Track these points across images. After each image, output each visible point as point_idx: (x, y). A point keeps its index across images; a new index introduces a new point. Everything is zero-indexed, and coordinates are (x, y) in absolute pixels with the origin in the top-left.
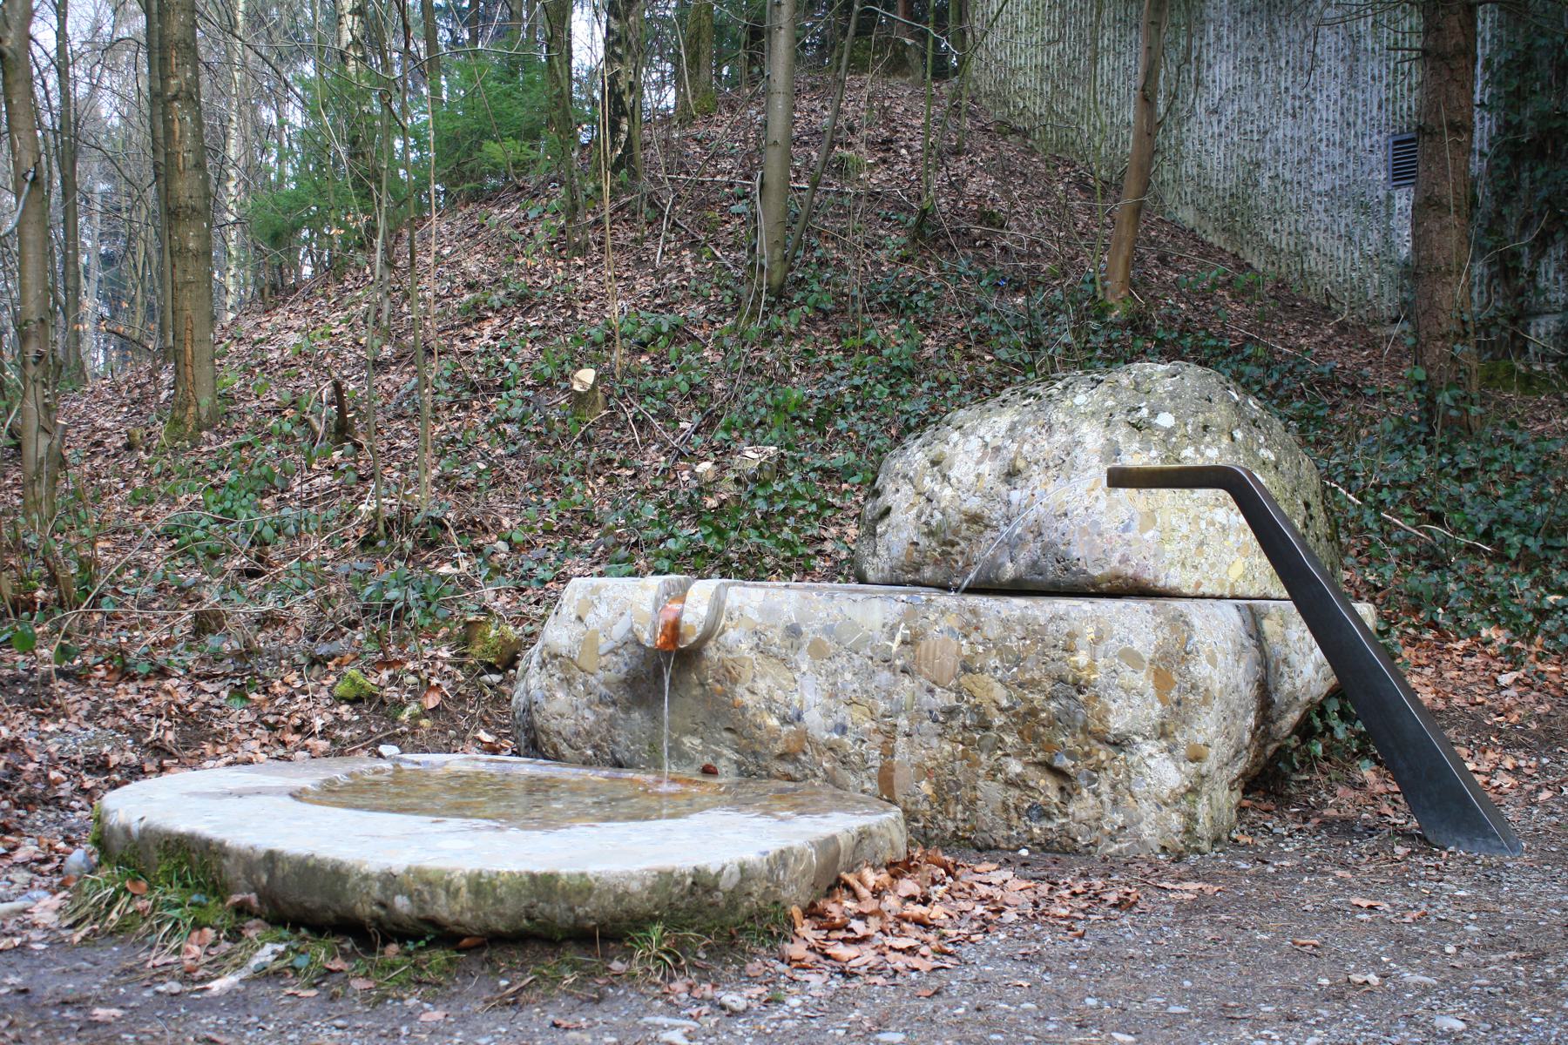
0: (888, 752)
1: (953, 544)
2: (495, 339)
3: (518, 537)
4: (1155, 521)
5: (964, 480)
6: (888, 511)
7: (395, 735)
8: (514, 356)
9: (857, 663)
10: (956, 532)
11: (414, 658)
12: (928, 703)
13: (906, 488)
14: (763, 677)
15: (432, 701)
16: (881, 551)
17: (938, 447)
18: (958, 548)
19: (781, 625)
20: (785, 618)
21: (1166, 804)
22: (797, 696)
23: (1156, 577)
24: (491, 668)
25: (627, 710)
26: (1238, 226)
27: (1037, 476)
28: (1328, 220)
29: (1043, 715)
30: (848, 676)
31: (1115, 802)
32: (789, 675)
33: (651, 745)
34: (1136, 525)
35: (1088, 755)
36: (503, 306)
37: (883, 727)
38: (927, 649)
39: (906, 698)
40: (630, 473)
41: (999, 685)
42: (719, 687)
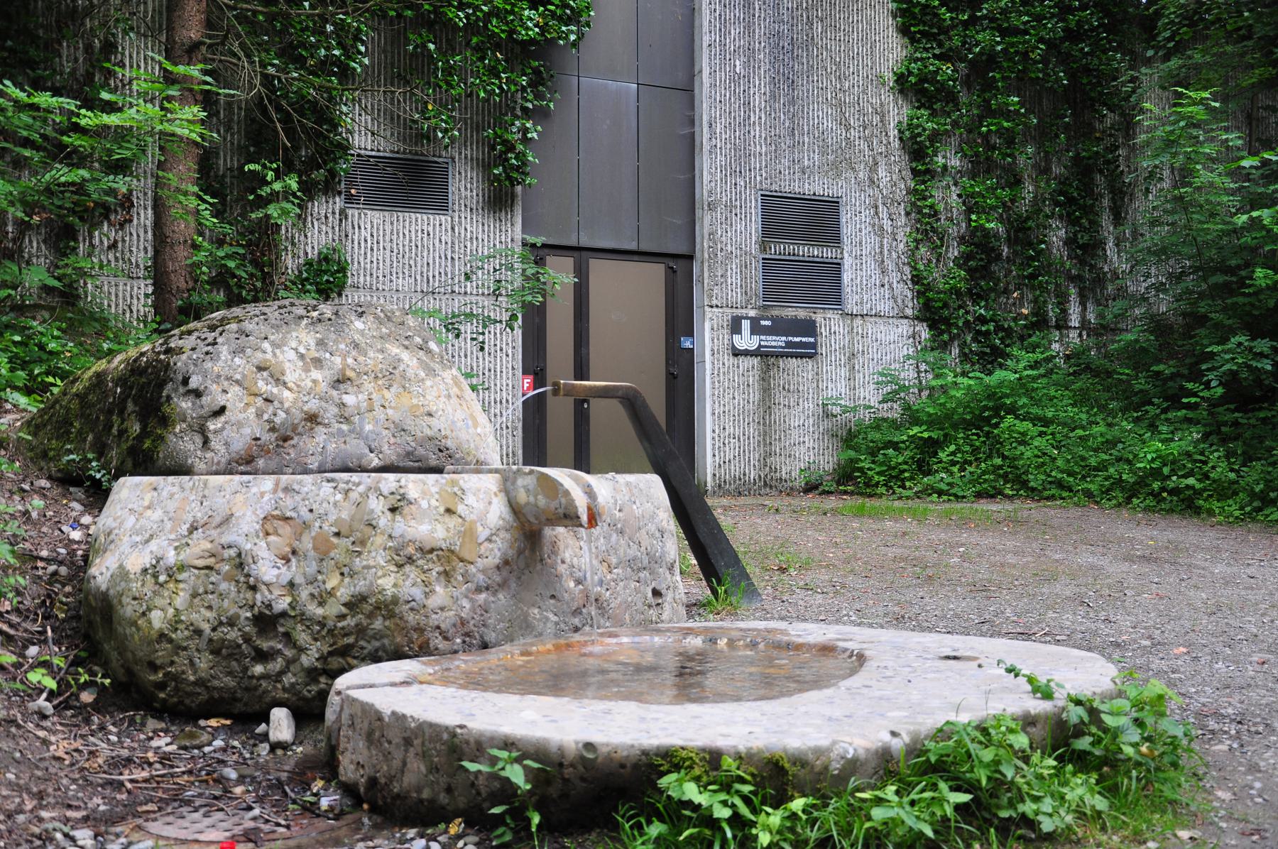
6: (222, 410)
16: (215, 443)
27: (369, 386)
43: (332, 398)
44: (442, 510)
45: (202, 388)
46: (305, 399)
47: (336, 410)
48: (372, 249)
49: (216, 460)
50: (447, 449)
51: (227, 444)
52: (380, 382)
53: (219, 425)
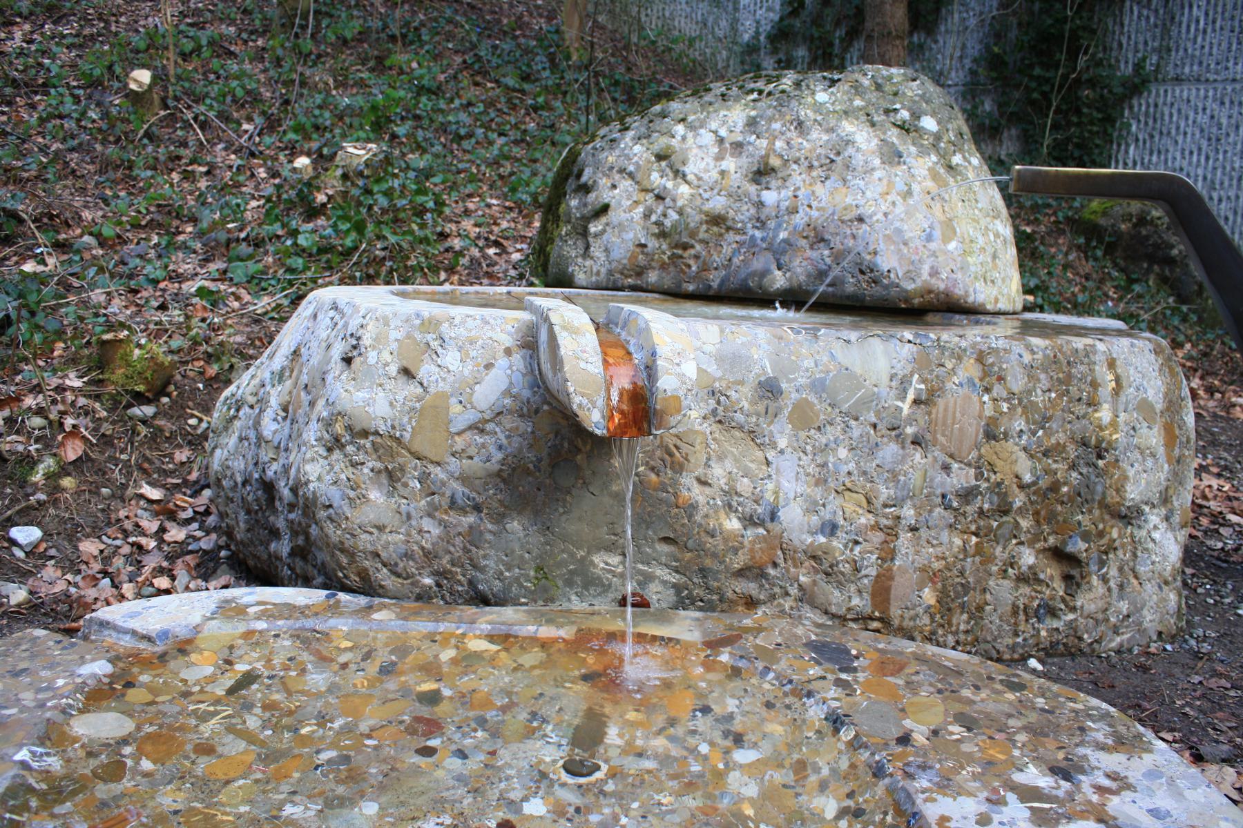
0: (888, 554)
1: (686, 247)
2: (28, 43)
3: (108, 231)
4: (955, 232)
5: (705, 176)
6: (605, 209)
7: (30, 508)
8: (53, 59)
9: (856, 433)
10: (693, 234)
11: (37, 389)
12: (943, 484)
13: (626, 184)
14: (720, 458)
15: (73, 451)
16: (596, 251)
17: (661, 142)
18: (692, 252)
19: (751, 379)
20: (757, 370)
21: (1166, 583)
22: (770, 486)
23: (966, 292)
24: (140, 399)
25: (499, 518)
26: (618, 10)
27: (798, 177)
28: (689, 10)
29: (1065, 489)
30: (843, 453)
31: (1121, 587)
32: (759, 454)
33: (539, 569)
34: (937, 233)
35: (1101, 534)
36: (31, 14)
37: (884, 522)
38: (946, 410)
39: (915, 479)
40: (203, 169)
41: (1022, 455)
42: (653, 477)
43: (747, 194)
44: (393, 369)
45: (590, 182)
46: (706, 196)
47: (753, 211)
48: (1205, 32)
49: (595, 270)
50: (872, 271)
51: (607, 250)
52: (814, 174)
53: (600, 228)
